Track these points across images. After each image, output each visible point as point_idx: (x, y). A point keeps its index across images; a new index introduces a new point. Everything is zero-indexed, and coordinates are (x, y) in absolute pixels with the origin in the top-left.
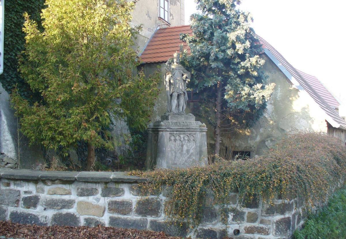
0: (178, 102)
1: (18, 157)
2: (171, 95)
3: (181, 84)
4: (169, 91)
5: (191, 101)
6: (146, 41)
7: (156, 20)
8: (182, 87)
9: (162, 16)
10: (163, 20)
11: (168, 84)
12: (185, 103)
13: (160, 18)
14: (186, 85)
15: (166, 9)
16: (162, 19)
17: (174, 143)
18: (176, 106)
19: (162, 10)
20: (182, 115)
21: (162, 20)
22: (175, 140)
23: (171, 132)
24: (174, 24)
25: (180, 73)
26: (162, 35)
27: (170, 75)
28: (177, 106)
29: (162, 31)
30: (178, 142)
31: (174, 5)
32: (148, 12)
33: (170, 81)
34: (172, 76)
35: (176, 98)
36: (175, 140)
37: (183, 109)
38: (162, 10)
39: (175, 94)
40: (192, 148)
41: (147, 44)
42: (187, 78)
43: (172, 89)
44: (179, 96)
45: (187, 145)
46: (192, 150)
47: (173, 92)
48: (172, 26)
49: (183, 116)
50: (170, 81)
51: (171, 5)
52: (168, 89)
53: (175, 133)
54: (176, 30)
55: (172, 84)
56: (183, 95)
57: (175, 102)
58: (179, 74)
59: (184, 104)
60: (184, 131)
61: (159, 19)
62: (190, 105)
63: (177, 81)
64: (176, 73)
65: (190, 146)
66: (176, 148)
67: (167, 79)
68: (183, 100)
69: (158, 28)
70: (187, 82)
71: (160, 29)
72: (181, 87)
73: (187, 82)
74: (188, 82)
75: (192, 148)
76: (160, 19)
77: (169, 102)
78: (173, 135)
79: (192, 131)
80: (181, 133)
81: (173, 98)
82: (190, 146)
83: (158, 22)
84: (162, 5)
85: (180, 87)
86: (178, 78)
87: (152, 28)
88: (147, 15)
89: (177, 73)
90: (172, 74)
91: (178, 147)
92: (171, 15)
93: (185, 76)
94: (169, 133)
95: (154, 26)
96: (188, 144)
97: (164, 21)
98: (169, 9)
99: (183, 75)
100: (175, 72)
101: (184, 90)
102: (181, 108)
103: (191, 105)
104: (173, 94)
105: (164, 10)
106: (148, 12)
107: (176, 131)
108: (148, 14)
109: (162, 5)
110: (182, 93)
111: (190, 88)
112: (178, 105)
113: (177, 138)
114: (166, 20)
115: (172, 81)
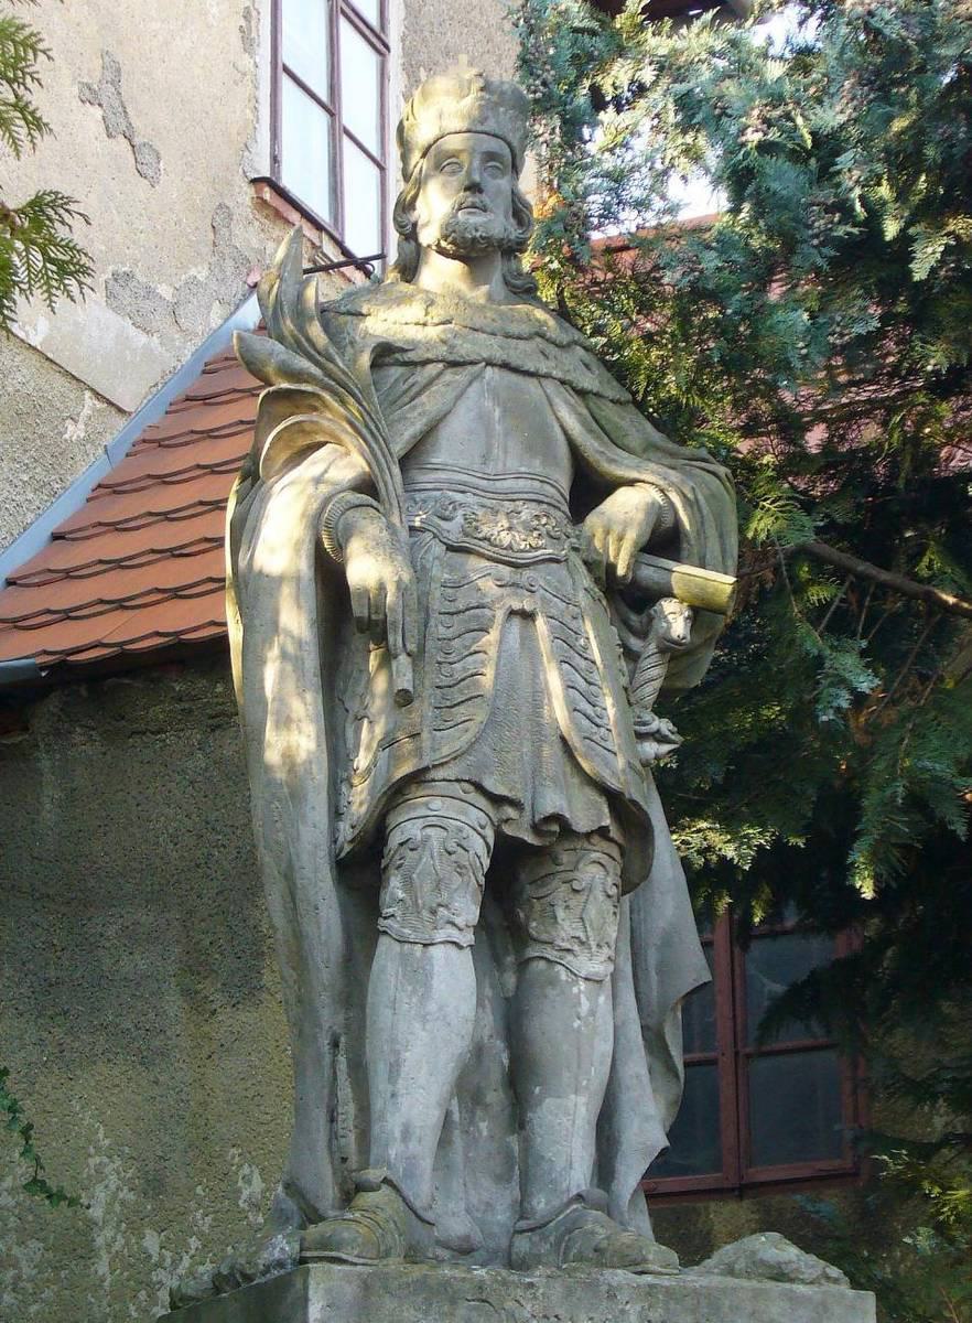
0: (514, 1018)
2: (364, 865)
3: (567, 638)
4: (320, 776)
5: (709, 1179)
6: (74, 432)
8: (582, 696)
10: (318, 226)
11: (295, 619)
12: (654, 1041)
13: (274, 196)
14: (653, 674)
15: (359, 113)
16: (307, 216)
18: (466, 1089)
20: (602, 1257)
21: (309, 231)
25: (537, 443)
27: (340, 463)
28: (495, 1096)
33: (329, 572)
34: (367, 486)
35: (467, 909)
37: (604, 1169)
38: (304, 127)
39: (446, 840)
41: (88, 471)
42: (664, 541)
43: (369, 735)
44: (515, 877)
47: (396, 794)
49: (621, 1276)
50: (329, 572)
52: (291, 737)
55: (377, 630)
56: (596, 872)
57: (432, 1002)
58: (511, 458)
59: (637, 1065)
63: (485, 579)
64: (459, 426)
67: (279, 544)
68: (597, 965)
70: (675, 619)
72: (568, 700)
73: (675, 619)
74: (701, 612)
76: (278, 215)
77: (329, 1017)
81: (394, 915)
85: (538, 696)
86: (499, 530)
87: (165, 291)
88: (90, 96)
89: (471, 433)
90: (370, 432)
93: (627, 509)
95: (200, 272)
99: (589, 489)
100: (430, 403)
101: (617, 768)
102: (566, 1125)
104: (407, 827)
105: (338, 132)
110: (587, 812)
111: (730, 822)
112: (509, 1075)
115: (366, 568)
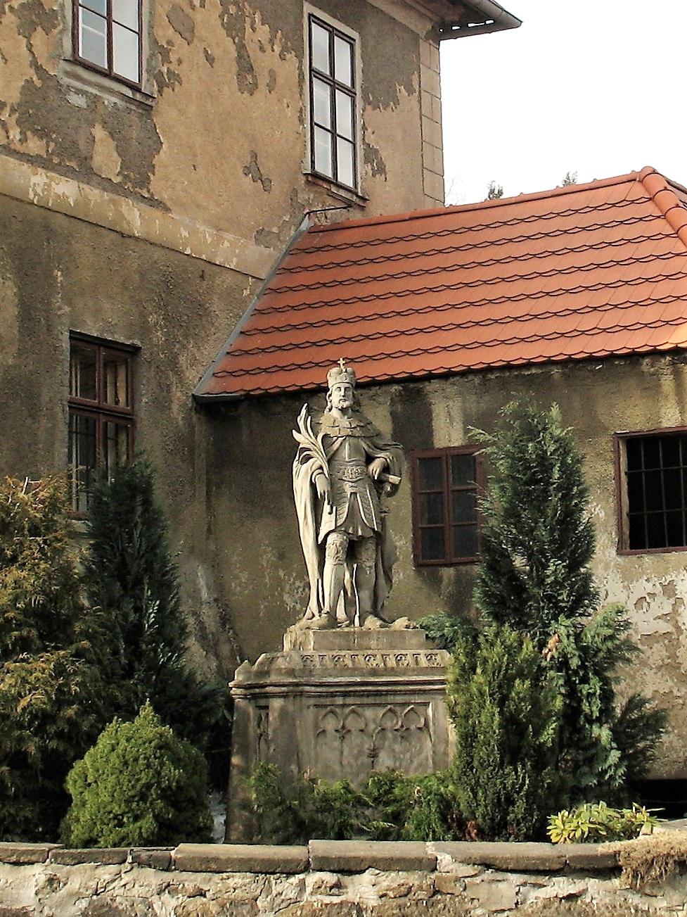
1: (71, 483)
6: (246, 293)
7: (295, 191)
9: (324, 168)
13: (315, 178)
15: (344, 127)
17: (337, 744)
19: (323, 141)
22: (343, 732)
23: (323, 701)
24: (388, 200)
26: (323, 258)
29: (318, 241)
30: (355, 739)
31: (386, 106)
32: (255, 156)
36: (343, 732)
38: (323, 141)
40: (415, 764)
45: (393, 750)
46: (416, 769)
48: (377, 210)
51: (369, 108)
53: (339, 701)
54: (382, 232)
60: (378, 694)
61: (308, 182)
62: (441, 580)
65: (408, 755)
66: (345, 762)
69: (306, 225)
71: (313, 231)
75: (415, 764)
76: (315, 184)
78: (332, 712)
79: (414, 692)
80: (365, 700)
82: (408, 755)
83: (305, 195)
84: (323, 117)
87: (275, 230)
91: (352, 761)
92: (371, 155)
94: (312, 701)
96: (397, 747)
97: (334, 189)
98: (359, 127)
99: (369, 459)
103: (445, 581)
106: (255, 156)
107: (345, 695)
108: (253, 170)
109: (323, 117)
113: (351, 723)
114: (346, 178)
